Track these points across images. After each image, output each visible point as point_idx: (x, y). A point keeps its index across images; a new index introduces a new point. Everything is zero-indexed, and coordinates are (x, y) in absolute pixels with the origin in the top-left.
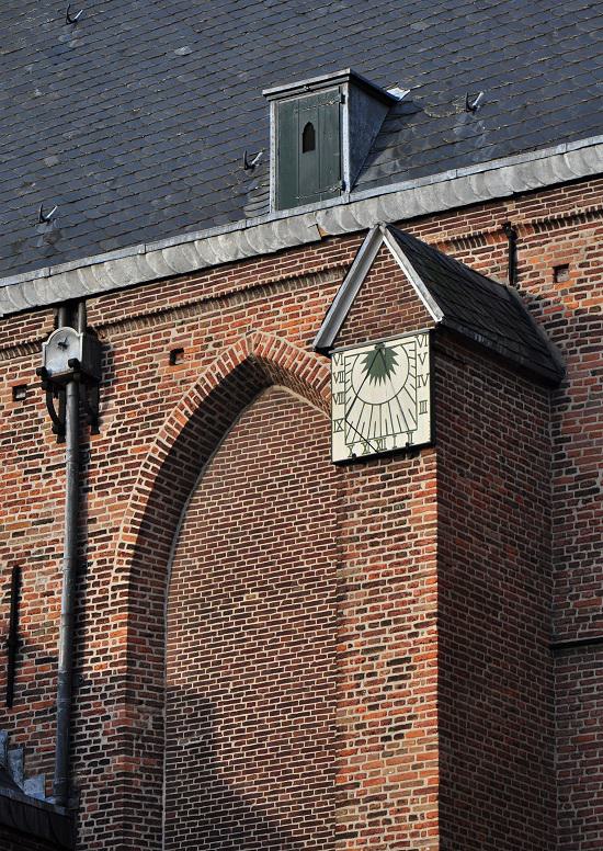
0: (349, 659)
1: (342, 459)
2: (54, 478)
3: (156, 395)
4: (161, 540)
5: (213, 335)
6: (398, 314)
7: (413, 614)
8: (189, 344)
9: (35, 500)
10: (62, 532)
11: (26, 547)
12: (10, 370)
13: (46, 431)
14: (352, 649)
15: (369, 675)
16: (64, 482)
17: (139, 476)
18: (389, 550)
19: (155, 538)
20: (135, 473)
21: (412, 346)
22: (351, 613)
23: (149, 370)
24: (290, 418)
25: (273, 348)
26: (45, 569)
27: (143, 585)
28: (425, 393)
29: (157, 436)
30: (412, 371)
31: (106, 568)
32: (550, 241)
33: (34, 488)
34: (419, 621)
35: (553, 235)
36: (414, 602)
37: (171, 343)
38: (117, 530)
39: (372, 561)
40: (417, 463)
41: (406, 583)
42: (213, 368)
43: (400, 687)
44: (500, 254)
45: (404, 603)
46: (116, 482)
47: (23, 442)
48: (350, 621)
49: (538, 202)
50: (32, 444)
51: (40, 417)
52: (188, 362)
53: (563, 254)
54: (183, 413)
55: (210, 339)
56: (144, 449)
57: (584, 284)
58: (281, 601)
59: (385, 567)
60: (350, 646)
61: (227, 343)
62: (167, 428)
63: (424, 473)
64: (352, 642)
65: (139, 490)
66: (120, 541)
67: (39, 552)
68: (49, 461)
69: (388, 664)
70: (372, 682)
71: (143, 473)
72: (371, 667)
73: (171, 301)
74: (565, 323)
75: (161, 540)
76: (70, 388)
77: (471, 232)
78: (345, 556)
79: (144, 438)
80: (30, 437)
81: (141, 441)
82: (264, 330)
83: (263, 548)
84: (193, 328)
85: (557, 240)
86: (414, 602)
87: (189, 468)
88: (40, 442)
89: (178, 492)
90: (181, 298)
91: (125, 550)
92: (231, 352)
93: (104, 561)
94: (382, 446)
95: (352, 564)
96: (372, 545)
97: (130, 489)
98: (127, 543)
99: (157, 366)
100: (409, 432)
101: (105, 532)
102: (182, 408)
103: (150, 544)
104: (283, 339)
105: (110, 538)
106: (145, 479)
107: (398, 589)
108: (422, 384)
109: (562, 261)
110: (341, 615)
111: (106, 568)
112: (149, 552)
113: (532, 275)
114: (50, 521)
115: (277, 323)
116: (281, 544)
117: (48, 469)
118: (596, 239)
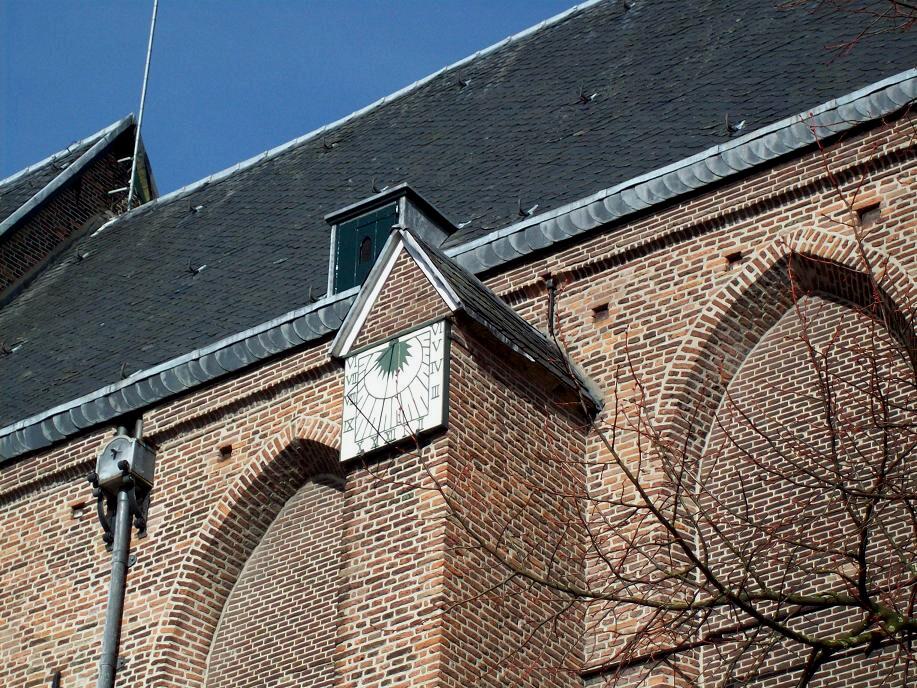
0: (347, 659)
1: (352, 456)
2: (101, 584)
3: (203, 492)
4: (200, 633)
5: (260, 429)
6: (416, 312)
7: (416, 602)
8: (237, 442)
9: (82, 608)
10: (100, 637)
11: (69, 653)
12: (71, 491)
13: (97, 543)
14: (351, 648)
15: (368, 672)
16: (108, 586)
17: (181, 570)
18: (395, 541)
19: (194, 631)
20: (177, 568)
21: (427, 336)
22: (352, 612)
23: (198, 470)
24: (332, 503)
25: (315, 429)
26: (85, 671)
27: (178, 677)
28: (438, 378)
29: (200, 530)
30: (426, 360)
31: (143, 662)
32: (590, 286)
33: (82, 597)
34: (423, 608)
35: (592, 280)
36: (418, 589)
37: (220, 442)
38: (155, 624)
39: (377, 555)
40: (428, 451)
41: (410, 572)
42: (258, 459)
43: (399, 679)
44: (540, 307)
45: (408, 592)
46: (158, 579)
47: (76, 555)
48: (352, 620)
49: (578, 249)
50: (85, 556)
51: (94, 530)
52: (237, 456)
53: (603, 295)
54: (226, 504)
55: (257, 432)
56: (189, 543)
57: (623, 319)
58: (314, 680)
59: (389, 559)
60: (350, 645)
61: (273, 433)
62: (211, 521)
63: (435, 459)
64: (352, 641)
65: (180, 583)
66: (159, 634)
67: (82, 655)
68: (98, 569)
69: (389, 658)
70: (370, 679)
71: (185, 567)
72: (370, 663)
73: (221, 401)
74: (603, 358)
75: (200, 633)
76: (123, 495)
77: (512, 289)
78: (350, 555)
79: (189, 534)
80: (83, 550)
81: (185, 537)
82: (308, 415)
83: (300, 630)
84: (242, 424)
85: (597, 284)
86: (418, 589)
87: (232, 562)
88: (92, 553)
89: (220, 587)
90: (230, 396)
91: (163, 642)
92: (276, 441)
93: (141, 656)
94: (391, 437)
95: (356, 562)
96: (378, 539)
97: (171, 584)
98: (165, 635)
99: (205, 465)
100: (421, 418)
101: (144, 628)
102: (225, 500)
103: (189, 637)
104: (326, 420)
105: (149, 633)
106: (186, 572)
107: (401, 579)
108: (435, 370)
109: (601, 302)
110: (341, 615)
111: (143, 662)
112: (187, 644)
113: (571, 321)
114: (94, 625)
115: (320, 406)
116: (317, 624)
117: (97, 577)
118: (636, 276)
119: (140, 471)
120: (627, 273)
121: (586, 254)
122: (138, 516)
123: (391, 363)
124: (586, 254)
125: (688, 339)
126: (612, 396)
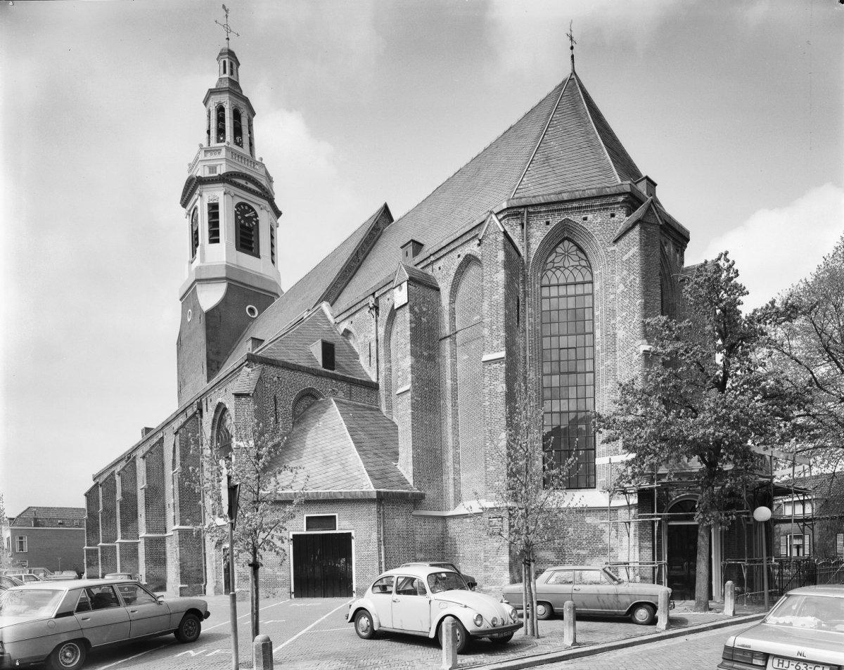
16: (374, 326)
119: (376, 305)
120: (443, 260)
121: (437, 256)
122: (377, 314)
123: (400, 290)
124: (437, 256)
125: (452, 273)
126: (441, 285)
